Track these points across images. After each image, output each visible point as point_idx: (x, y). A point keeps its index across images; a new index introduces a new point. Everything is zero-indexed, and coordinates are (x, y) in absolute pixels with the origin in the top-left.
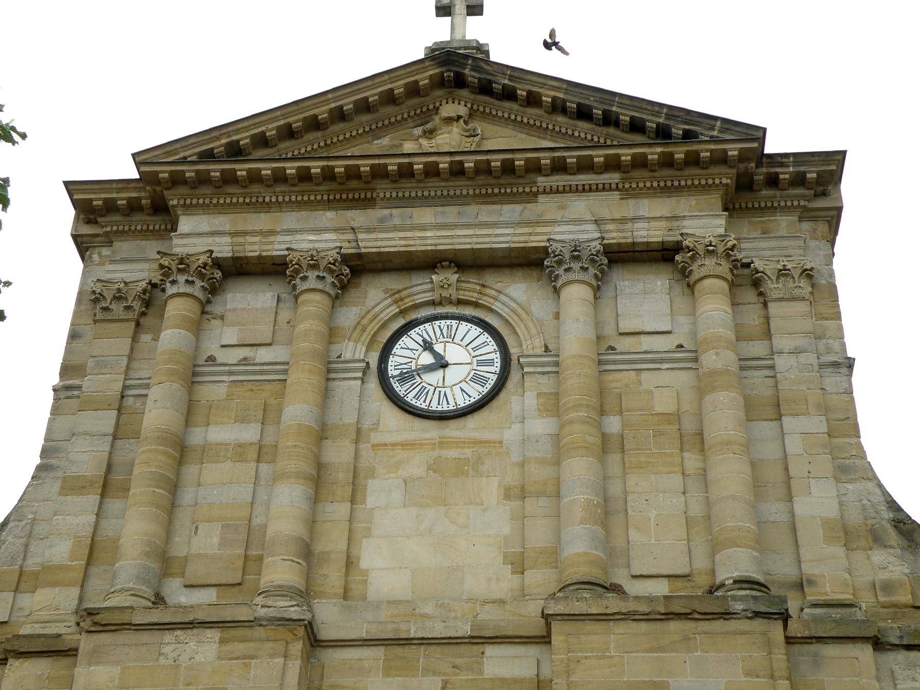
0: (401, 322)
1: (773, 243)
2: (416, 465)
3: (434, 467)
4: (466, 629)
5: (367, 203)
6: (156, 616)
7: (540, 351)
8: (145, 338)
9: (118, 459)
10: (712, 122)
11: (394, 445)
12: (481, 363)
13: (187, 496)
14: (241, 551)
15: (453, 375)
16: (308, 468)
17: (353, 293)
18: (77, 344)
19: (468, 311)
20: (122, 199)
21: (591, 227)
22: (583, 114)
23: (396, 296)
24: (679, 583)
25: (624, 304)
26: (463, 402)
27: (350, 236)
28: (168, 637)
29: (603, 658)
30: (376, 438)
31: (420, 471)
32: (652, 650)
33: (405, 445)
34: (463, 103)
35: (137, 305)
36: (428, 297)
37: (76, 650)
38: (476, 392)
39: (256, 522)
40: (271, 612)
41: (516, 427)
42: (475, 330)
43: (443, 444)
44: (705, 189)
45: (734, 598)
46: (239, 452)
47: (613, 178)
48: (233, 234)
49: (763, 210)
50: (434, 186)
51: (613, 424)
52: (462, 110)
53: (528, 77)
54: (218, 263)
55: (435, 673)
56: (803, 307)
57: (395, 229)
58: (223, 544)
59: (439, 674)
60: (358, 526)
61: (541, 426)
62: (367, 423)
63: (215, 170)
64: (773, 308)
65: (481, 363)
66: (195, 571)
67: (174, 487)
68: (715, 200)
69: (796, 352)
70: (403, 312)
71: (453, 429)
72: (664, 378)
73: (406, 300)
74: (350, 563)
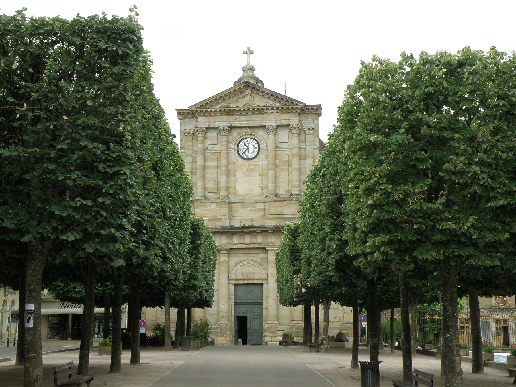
0: (240, 139)
1: (307, 121)
2: (244, 169)
4: (254, 201)
5: (232, 115)
6: (205, 201)
7: (265, 147)
8: (194, 141)
9: (193, 167)
12: (255, 148)
13: (206, 176)
14: (216, 186)
15: (250, 150)
16: (226, 173)
17: (231, 133)
18: (182, 142)
19: (252, 137)
21: (274, 121)
23: (239, 134)
24: (287, 192)
25: (280, 136)
26: (252, 157)
27: (230, 123)
28: (208, 204)
30: (237, 164)
31: (245, 171)
33: (242, 165)
35: (192, 134)
36: (245, 134)
37: (245, 342)
38: (254, 154)
39: (219, 181)
40: (223, 200)
41: (261, 162)
42: (254, 141)
43: (249, 165)
44: (295, 113)
45: (294, 198)
46: (214, 167)
47: (278, 111)
48: (208, 122)
49: (306, 114)
50: (245, 112)
51: (277, 162)
52: (250, 92)
54: (206, 128)
56: (312, 136)
57: (238, 121)
58: (213, 185)
60: (235, 181)
61: (265, 162)
62: (235, 161)
64: (307, 136)
65: (255, 148)
66: (210, 190)
67: (204, 175)
68: (297, 114)
69: (310, 146)
70: (241, 137)
71: (251, 162)
72: (287, 152)
74: (234, 188)
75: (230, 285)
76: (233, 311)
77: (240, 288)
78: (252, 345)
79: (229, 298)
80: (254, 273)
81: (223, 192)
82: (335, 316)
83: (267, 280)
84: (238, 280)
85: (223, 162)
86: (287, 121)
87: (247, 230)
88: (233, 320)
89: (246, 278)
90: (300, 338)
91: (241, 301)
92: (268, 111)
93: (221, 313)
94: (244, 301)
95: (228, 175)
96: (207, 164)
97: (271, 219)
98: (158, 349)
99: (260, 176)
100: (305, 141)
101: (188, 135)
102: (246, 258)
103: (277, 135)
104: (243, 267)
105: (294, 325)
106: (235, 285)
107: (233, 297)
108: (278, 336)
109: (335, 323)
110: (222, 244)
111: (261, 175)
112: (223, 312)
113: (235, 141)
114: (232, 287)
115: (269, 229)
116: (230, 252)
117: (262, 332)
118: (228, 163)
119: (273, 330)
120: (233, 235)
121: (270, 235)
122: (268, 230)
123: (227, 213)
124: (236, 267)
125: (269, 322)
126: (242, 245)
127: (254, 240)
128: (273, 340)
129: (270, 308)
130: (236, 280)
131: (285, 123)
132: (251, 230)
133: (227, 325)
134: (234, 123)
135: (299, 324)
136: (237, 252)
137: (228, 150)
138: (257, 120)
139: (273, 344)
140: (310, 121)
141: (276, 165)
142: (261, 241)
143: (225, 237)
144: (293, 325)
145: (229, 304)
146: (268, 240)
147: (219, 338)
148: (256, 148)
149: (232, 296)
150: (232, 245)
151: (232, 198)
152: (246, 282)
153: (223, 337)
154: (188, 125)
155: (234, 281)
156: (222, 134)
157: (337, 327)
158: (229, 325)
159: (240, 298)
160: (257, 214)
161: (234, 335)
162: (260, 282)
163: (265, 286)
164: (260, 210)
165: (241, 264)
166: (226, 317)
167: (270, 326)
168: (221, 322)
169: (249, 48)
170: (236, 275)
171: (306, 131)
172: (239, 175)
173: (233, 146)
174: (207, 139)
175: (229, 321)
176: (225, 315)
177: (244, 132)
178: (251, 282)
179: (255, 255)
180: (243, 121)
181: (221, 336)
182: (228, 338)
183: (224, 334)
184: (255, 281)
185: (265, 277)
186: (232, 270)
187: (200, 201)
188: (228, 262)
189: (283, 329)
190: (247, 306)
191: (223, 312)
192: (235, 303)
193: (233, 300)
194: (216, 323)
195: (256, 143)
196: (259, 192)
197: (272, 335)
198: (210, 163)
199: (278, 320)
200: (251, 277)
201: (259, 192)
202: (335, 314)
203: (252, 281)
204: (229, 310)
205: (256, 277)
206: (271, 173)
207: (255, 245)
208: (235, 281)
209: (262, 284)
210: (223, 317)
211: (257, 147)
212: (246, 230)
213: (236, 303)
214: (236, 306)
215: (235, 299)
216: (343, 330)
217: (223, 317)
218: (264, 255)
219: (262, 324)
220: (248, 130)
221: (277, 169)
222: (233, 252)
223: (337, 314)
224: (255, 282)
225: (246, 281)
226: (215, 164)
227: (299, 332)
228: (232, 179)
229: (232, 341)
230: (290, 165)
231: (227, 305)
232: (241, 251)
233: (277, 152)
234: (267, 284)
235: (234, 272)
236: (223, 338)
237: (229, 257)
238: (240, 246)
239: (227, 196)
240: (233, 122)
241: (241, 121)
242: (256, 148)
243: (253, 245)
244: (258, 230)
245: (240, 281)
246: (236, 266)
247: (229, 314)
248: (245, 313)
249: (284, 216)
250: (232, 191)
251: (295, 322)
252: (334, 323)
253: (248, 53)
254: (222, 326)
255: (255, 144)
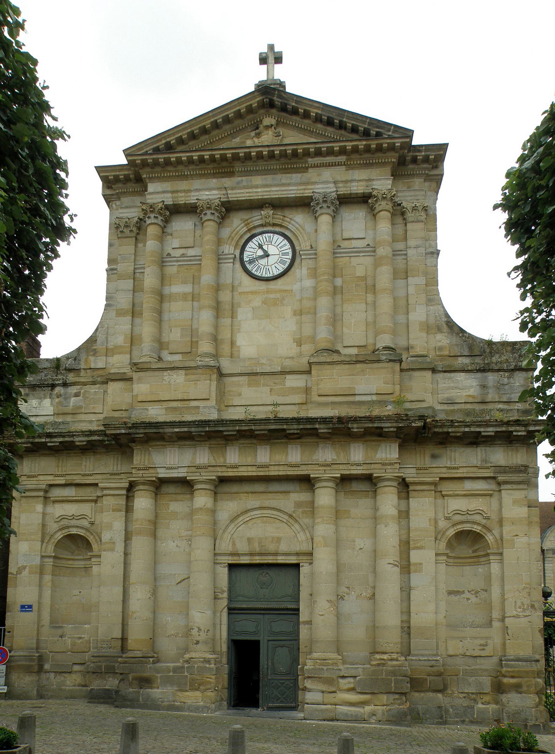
0: (248, 235)
1: (412, 193)
2: (257, 301)
3: (264, 302)
4: (279, 369)
6: (159, 365)
7: (309, 248)
9: (136, 301)
10: (389, 127)
11: (248, 292)
13: (166, 317)
17: (227, 221)
19: (277, 229)
20: (122, 174)
21: (332, 185)
22: (330, 123)
24: (362, 349)
25: (346, 225)
26: (276, 273)
27: (224, 192)
28: (165, 373)
29: (331, 379)
30: (240, 290)
32: (349, 375)
33: (252, 293)
34: (273, 117)
35: (134, 229)
36: (260, 222)
38: (281, 268)
39: (194, 327)
42: (281, 239)
43: (268, 292)
45: (382, 354)
46: (184, 297)
47: (342, 158)
53: (305, 101)
55: (267, 386)
56: (421, 225)
59: (269, 386)
61: (309, 283)
62: (236, 283)
63: (161, 158)
64: (409, 226)
65: (284, 254)
66: (173, 347)
67: (160, 313)
68: (388, 170)
69: (417, 247)
70: (249, 230)
71: (272, 285)
73: (251, 224)
74: (233, 343)
75: (218, 567)
76: (225, 628)
77: (242, 576)
78: (270, 709)
79: (216, 598)
80: (279, 540)
81: (205, 347)
82: (483, 642)
83: (311, 554)
84: (238, 555)
85: (207, 278)
86: (364, 183)
87: (262, 427)
88: (225, 648)
89: (258, 550)
90: (397, 696)
91: (244, 606)
92: (318, 160)
93: (195, 632)
94: (251, 606)
95: (217, 308)
96: (167, 290)
97: (326, 404)
98: (233, 657)
99: (295, 314)
100: (405, 239)
101: (127, 231)
102: (257, 504)
103: (338, 219)
104: (250, 524)
105: (384, 665)
106: (231, 567)
107: (225, 595)
108: (340, 690)
109: (482, 660)
110: (198, 467)
111: (299, 313)
112: (200, 630)
113: (237, 237)
114: (223, 572)
115: (320, 423)
116: (220, 489)
117: (296, 680)
118: (218, 288)
119: (326, 675)
120: (226, 445)
121: (321, 446)
122: (317, 426)
123: (214, 394)
124: (232, 525)
125: (315, 655)
126: (250, 468)
127: (279, 458)
128: (326, 701)
129: (318, 620)
130: (232, 554)
131: (358, 188)
132: (273, 427)
133: (208, 661)
134: (234, 191)
135: (395, 663)
136: (235, 488)
137: (219, 259)
138: (289, 185)
139: (327, 710)
140: (417, 193)
141: (335, 287)
142: (299, 460)
143: (207, 450)
144: (379, 665)
145: (214, 613)
146: (315, 457)
147: (187, 693)
148: (287, 254)
149: (222, 592)
150: (224, 469)
151: (227, 365)
152: (257, 560)
153: (196, 690)
154: (126, 211)
155: (227, 558)
156: (205, 218)
157: (486, 670)
158: (213, 662)
159: (240, 598)
160: (288, 400)
161: (226, 684)
162: (292, 560)
163: (304, 570)
164: (294, 390)
165: (246, 517)
166: (206, 642)
167: (321, 664)
168: (193, 655)
169: (271, 47)
170: (234, 544)
171: (410, 216)
172: (244, 313)
173: (229, 249)
174: (169, 237)
175: (214, 652)
176: (203, 637)
177: (257, 217)
178: (270, 560)
179: (281, 496)
180: (257, 187)
181: (194, 688)
182: (211, 694)
183: (200, 685)
184: (280, 558)
185: (305, 547)
186: (224, 531)
187: (145, 366)
188: (213, 512)
189: (353, 672)
190: (261, 616)
191: (200, 630)
192: (230, 609)
193: (225, 603)
194: (182, 655)
195: (285, 242)
196: (294, 350)
197: (324, 688)
198: (176, 289)
199: (338, 651)
200: (272, 548)
201: (294, 350)
202: (482, 638)
203: (274, 558)
204: (214, 625)
205: (283, 548)
206: (324, 302)
207: (281, 468)
208: (230, 558)
209: (297, 566)
210: (197, 643)
211: (290, 251)
212: (258, 428)
213: (231, 611)
214: (232, 616)
215: (230, 599)
216: (505, 676)
217: (197, 643)
218: (301, 496)
219: (296, 661)
220: (268, 212)
221: (339, 297)
222: (226, 488)
223: (487, 638)
224: (281, 560)
225: (257, 558)
226: (188, 289)
227: (396, 681)
228: (226, 321)
229: (222, 700)
230: (373, 289)
231: (209, 613)
232: (247, 487)
233: (338, 260)
234: (311, 564)
235: (227, 536)
236: (198, 694)
237: (215, 500)
238: (243, 472)
239: (216, 356)
240: (233, 189)
241: (252, 187)
242: (287, 254)
243: (276, 468)
244: (291, 427)
245: (242, 558)
246: (232, 521)
247: (214, 635)
248: (255, 633)
249: (357, 398)
250: (226, 349)
251: (385, 657)
252: (478, 660)
253: (271, 60)
254: (195, 663)
255: (285, 245)
